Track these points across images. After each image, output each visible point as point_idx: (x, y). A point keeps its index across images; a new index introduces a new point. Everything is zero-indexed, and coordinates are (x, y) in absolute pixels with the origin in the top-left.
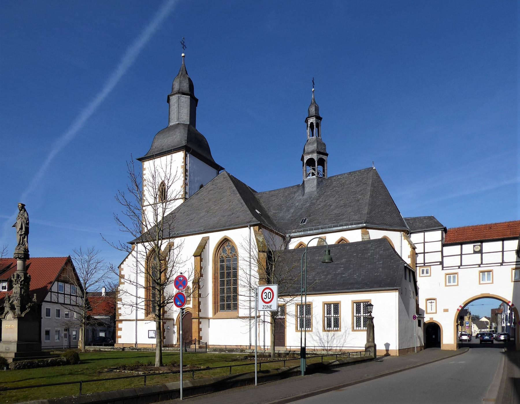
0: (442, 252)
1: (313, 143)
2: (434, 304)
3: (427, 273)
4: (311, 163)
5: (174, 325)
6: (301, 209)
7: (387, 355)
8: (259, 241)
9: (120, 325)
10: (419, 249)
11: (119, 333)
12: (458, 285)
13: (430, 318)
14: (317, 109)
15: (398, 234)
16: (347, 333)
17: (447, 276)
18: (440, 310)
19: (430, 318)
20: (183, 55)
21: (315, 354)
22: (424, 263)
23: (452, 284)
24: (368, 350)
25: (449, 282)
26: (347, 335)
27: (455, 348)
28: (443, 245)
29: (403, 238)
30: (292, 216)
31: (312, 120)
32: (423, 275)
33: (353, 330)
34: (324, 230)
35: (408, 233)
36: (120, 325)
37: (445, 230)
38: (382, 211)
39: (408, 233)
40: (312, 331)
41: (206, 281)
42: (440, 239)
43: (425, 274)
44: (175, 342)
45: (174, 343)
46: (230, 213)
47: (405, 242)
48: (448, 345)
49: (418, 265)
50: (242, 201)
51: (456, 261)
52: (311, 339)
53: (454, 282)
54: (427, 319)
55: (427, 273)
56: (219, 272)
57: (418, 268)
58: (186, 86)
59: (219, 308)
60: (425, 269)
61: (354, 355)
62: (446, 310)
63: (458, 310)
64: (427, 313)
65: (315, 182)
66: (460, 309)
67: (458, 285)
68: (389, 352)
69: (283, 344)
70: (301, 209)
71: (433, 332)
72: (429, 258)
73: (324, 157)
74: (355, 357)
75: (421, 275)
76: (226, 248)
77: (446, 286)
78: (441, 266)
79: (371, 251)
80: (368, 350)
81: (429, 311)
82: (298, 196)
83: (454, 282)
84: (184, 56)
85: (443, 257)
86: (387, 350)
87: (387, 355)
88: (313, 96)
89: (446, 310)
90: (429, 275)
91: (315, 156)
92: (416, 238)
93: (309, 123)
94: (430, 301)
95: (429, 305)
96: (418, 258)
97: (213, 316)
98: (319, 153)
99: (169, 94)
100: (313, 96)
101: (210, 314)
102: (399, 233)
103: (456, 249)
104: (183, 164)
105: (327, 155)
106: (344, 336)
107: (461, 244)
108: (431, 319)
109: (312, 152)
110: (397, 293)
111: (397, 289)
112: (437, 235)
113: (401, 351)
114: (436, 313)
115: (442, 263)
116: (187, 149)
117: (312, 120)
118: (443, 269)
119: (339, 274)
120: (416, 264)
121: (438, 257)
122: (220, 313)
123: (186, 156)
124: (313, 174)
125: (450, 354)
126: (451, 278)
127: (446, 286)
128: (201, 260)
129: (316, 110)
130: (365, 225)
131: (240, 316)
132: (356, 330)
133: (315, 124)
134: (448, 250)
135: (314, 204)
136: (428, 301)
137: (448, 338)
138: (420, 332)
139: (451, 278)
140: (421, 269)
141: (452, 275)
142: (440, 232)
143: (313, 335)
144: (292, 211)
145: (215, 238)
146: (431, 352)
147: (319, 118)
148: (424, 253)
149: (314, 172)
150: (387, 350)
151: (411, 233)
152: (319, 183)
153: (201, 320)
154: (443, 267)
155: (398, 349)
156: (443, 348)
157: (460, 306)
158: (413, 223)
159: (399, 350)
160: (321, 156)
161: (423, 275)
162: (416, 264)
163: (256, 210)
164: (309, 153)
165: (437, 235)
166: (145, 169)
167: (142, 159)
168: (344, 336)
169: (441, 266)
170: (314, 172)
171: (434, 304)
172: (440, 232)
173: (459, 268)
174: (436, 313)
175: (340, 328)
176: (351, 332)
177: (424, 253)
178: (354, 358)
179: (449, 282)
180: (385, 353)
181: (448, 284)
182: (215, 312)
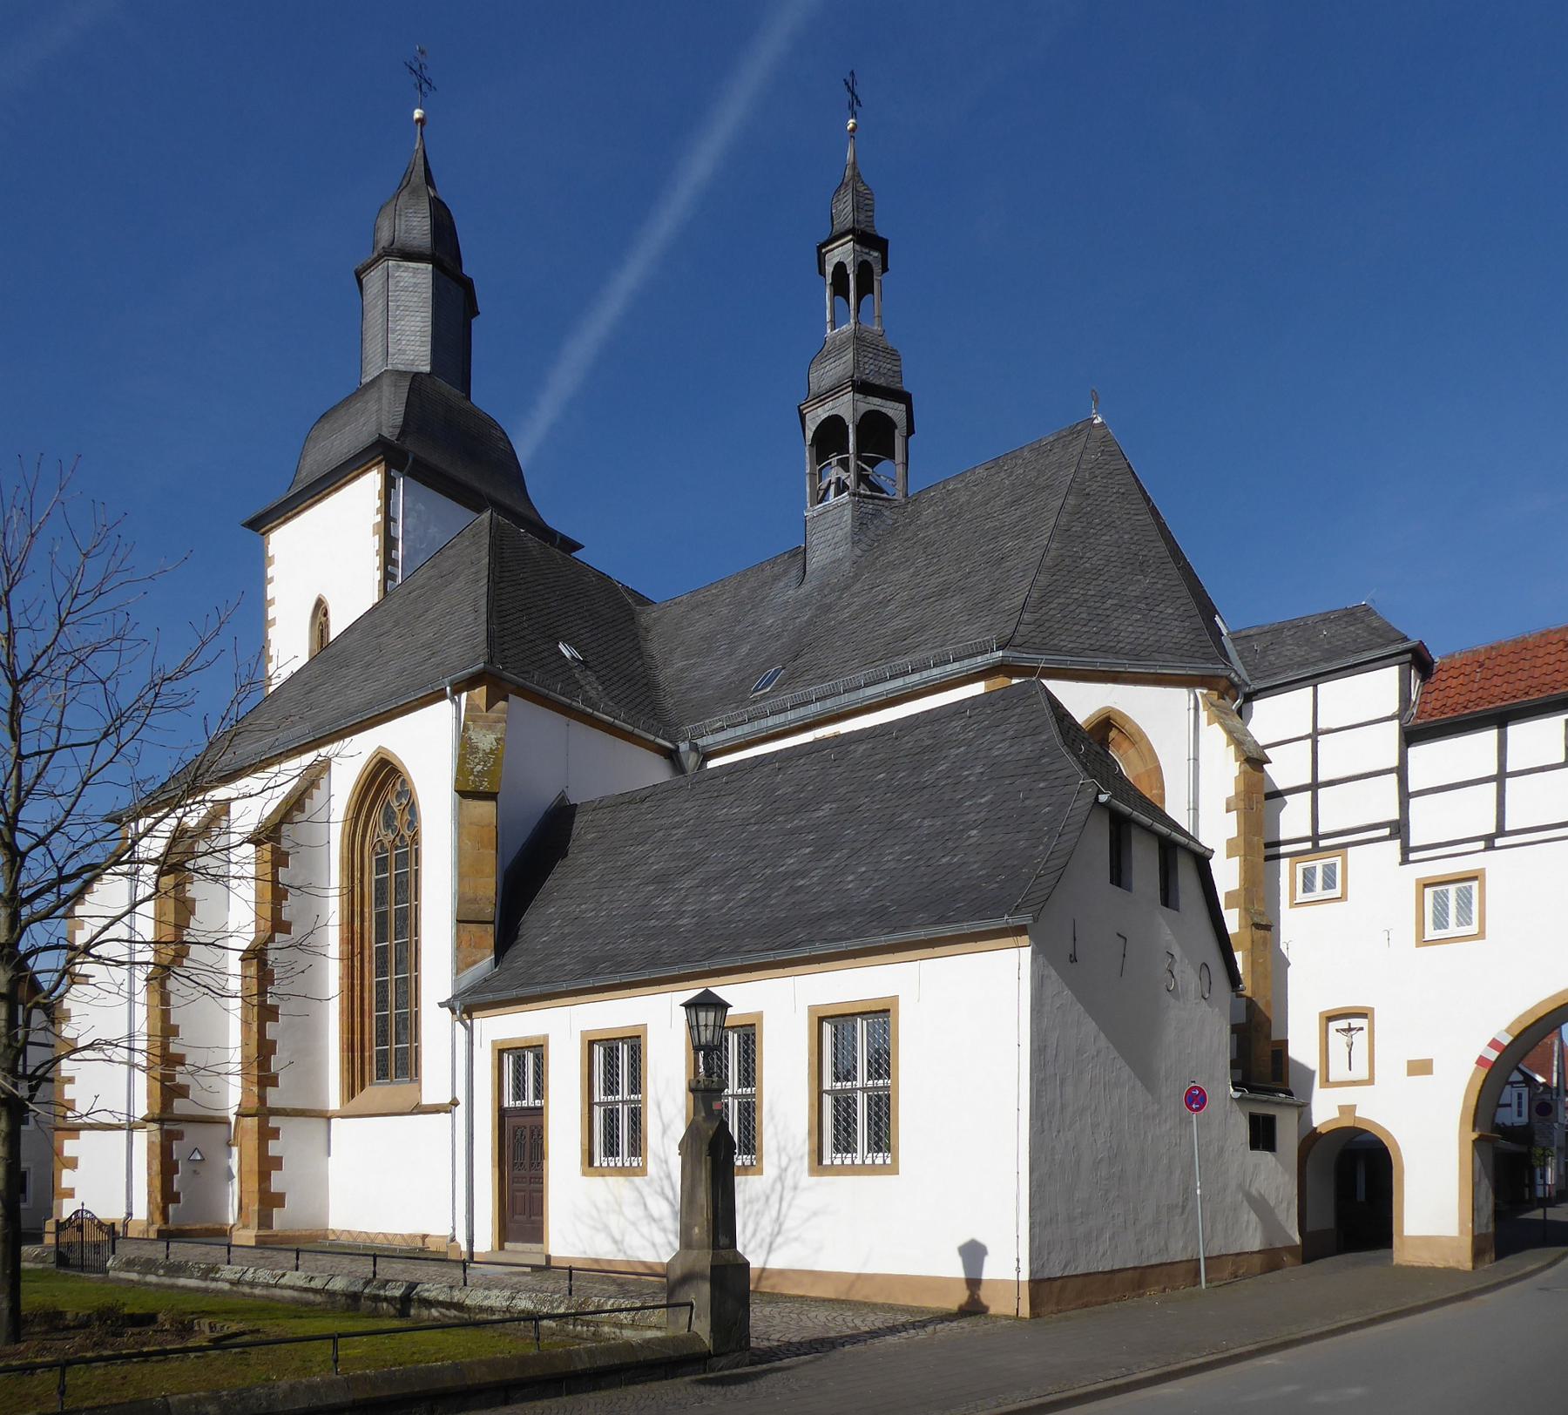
0: (1401, 771)
1: (839, 349)
2: (1360, 1039)
3: (1329, 883)
4: (829, 437)
5: (229, 1145)
6: (779, 636)
7: (973, 1308)
8: (474, 750)
9: (70, 1147)
10: (1285, 769)
11: (67, 1178)
12: (1481, 935)
13: (1342, 1109)
14: (862, 204)
15: (1180, 698)
16: (789, 1182)
17: (1429, 892)
18: (1391, 1064)
19: (1342, 1109)
20: (417, 114)
21: (459, 1306)
22: (1315, 837)
23: (1453, 930)
24: (681, 1297)
25: (1441, 923)
26: (788, 1196)
27: (1463, 1259)
28: (1412, 736)
29: (1203, 715)
30: (737, 671)
31: (843, 253)
32: (1310, 897)
33: (817, 1163)
34: (830, 704)
35: (1233, 694)
36: (70, 1147)
37: (1419, 662)
38: (1109, 595)
39: (1233, 694)
40: (641, 1171)
41: (308, 947)
42: (1393, 706)
43: (1319, 892)
44: (232, 1217)
45: (231, 1222)
46: (426, 653)
47: (1214, 737)
48: (1427, 1241)
49: (1283, 849)
50: (484, 601)
51: (1476, 811)
52: (640, 1212)
53: (1464, 918)
54: (1324, 1110)
55: (1329, 883)
56: (370, 912)
57: (1285, 863)
58: (416, 227)
59: (372, 1069)
60: (1319, 865)
61: (621, 1326)
62: (1420, 1068)
63: (1481, 1061)
64: (1326, 1082)
65: (848, 514)
66: (1493, 1055)
67: (1481, 935)
68: (985, 1295)
69: (536, 1233)
70: (779, 636)
71: (1356, 1177)
72: (1339, 809)
73: (895, 411)
74: (628, 1334)
75: (1301, 896)
76: (394, 804)
77: (1422, 941)
78: (1396, 844)
79: (954, 752)
80: (681, 1297)
81: (1338, 1071)
82: (787, 592)
83: (1464, 918)
84: (421, 121)
85: (1405, 796)
86: (974, 1283)
87: (973, 1308)
88: (850, 155)
89: (1420, 1068)
90: (1337, 892)
91: (846, 407)
92: (1274, 717)
93: (829, 269)
94: (1343, 1024)
95: (1337, 1042)
96: (1283, 816)
97: (342, 1104)
98: (863, 388)
99: (358, 266)
100: (850, 155)
101: (334, 1101)
102: (1184, 692)
103: (1472, 752)
104: (379, 518)
105: (904, 398)
106: (775, 1198)
107: (1501, 719)
108: (1347, 1110)
109: (833, 391)
110: (1027, 952)
111: (1019, 931)
112: (1379, 689)
113: (1044, 1289)
114: (1370, 1081)
115: (1399, 829)
116: (387, 455)
117: (843, 253)
118: (1405, 861)
119: (786, 876)
120: (1279, 844)
121: (1380, 802)
122: (376, 1093)
123: (389, 485)
124: (841, 487)
125: (1434, 1289)
126: (1450, 903)
127: (1422, 941)
128: (280, 860)
129: (857, 208)
130: (1000, 653)
131: (425, 1101)
132: (835, 1170)
133: (850, 270)
134: (1435, 760)
135: (828, 608)
136: (1333, 1025)
137: (1434, 1202)
138: (1275, 1177)
139: (1450, 903)
140: (1300, 868)
141: (1452, 889)
142: (1391, 674)
143: (646, 1191)
144: (744, 649)
145: (348, 761)
146: (1343, 1276)
147: (866, 239)
148: (1314, 786)
149: (844, 475)
150: (974, 1283)
151: (1250, 698)
152: (861, 523)
153: (274, 1122)
154: (1406, 850)
155: (1025, 1276)
156: (1402, 1255)
157: (1494, 1044)
158: (1265, 650)
159: (1036, 1284)
160: (875, 403)
161: (1310, 897)
162: (1279, 844)
163: (561, 646)
164: (822, 398)
165: (1379, 689)
166: (270, 561)
167: (263, 522)
168: (775, 1198)
169: (1396, 844)
170: (844, 475)
171: (1360, 1039)
172: (1391, 674)
173: (1490, 847)
174: (1370, 1081)
175: (760, 1159)
176: (806, 1180)
177: (1314, 786)
178: (629, 1346)
179: (1441, 923)
180: (960, 1297)
181: (1431, 933)
182: (352, 1087)
